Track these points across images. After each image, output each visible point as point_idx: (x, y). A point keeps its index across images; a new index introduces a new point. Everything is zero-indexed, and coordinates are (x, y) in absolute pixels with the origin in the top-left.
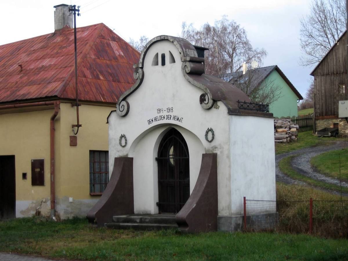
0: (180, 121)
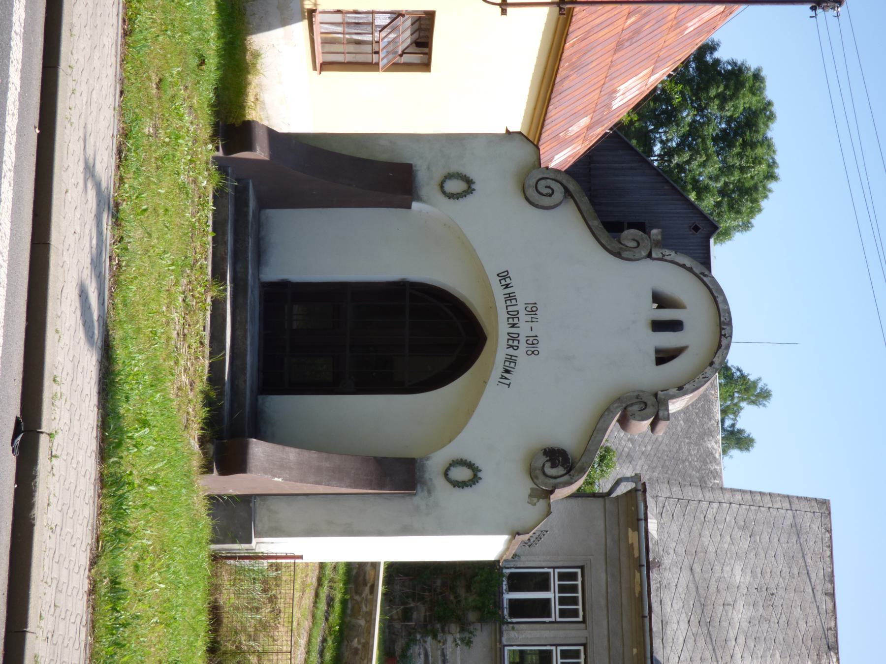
0: (502, 377)
